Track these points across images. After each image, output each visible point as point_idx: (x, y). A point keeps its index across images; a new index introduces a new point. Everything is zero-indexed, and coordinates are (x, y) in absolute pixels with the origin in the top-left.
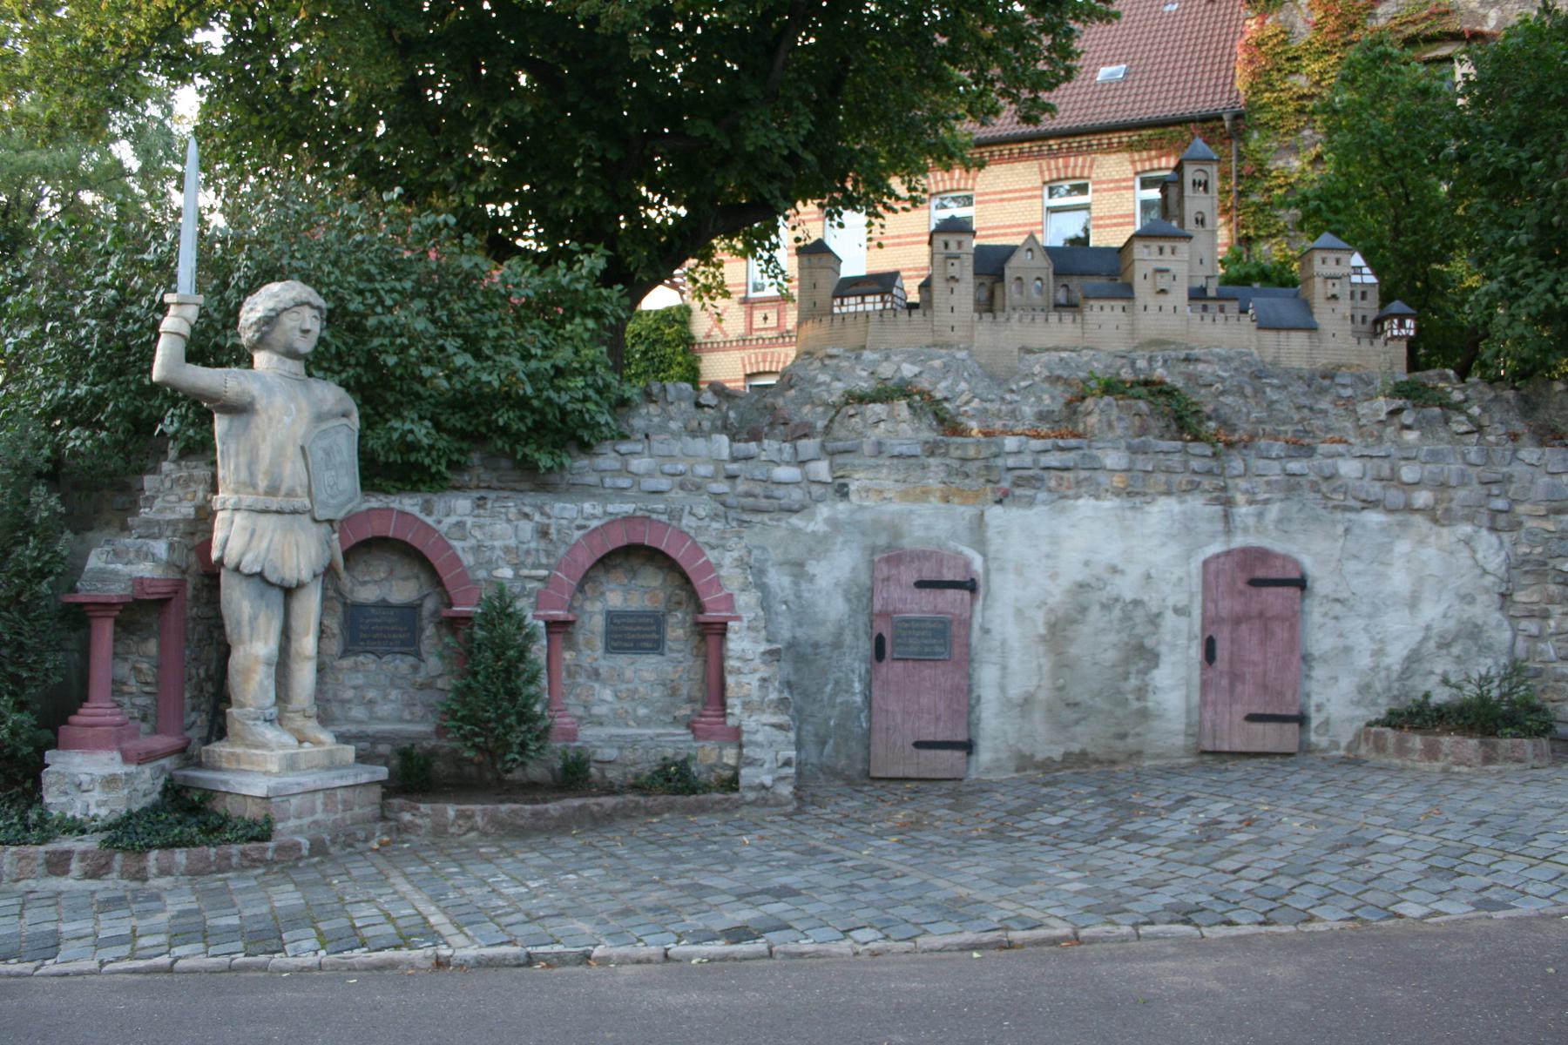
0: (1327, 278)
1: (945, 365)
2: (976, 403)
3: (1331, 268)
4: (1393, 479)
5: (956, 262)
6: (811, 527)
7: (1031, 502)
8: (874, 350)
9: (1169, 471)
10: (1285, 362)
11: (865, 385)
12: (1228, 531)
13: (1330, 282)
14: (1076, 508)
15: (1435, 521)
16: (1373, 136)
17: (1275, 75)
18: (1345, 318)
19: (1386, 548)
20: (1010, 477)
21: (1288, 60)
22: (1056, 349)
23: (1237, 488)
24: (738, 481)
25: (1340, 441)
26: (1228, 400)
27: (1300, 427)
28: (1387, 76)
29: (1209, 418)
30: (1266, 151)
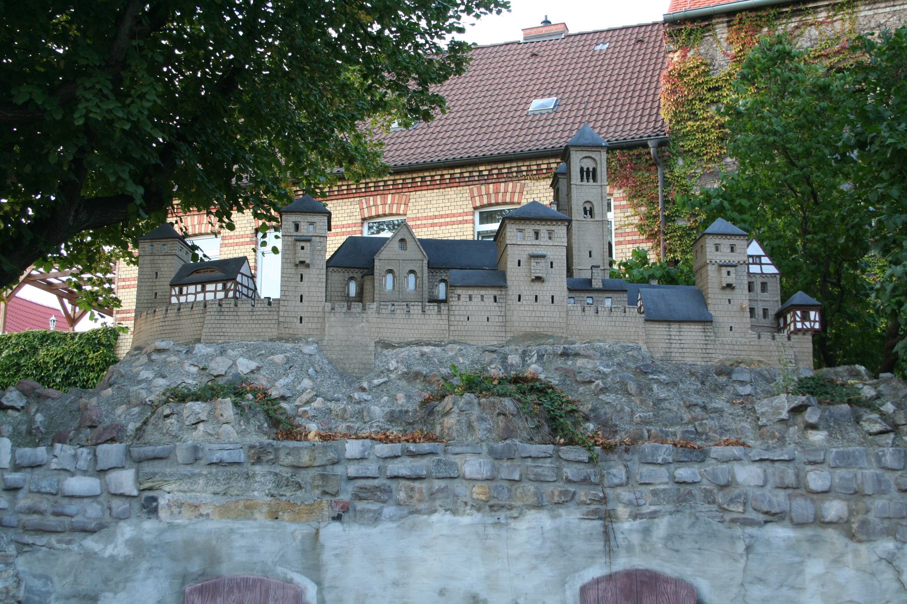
0: (721, 266)
1: (288, 360)
2: (318, 403)
3: (724, 255)
4: (798, 487)
5: (307, 245)
6: (109, 551)
7: (376, 518)
8: (209, 343)
9: (539, 480)
10: (676, 357)
11: (191, 380)
12: (609, 551)
13: (724, 270)
14: (430, 525)
15: (852, 536)
16: (775, 133)
17: (698, 105)
18: (742, 309)
19: (797, 569)
20: (350, 488)
21: (709, 90)
22: (418, 343)
23: (618, 499)
24: (21, 494)
25: (737, 443)
26: (610, 398)
27: (690, 428)
28: (787, 74)
29: (587, 419)
30: (691, 177)
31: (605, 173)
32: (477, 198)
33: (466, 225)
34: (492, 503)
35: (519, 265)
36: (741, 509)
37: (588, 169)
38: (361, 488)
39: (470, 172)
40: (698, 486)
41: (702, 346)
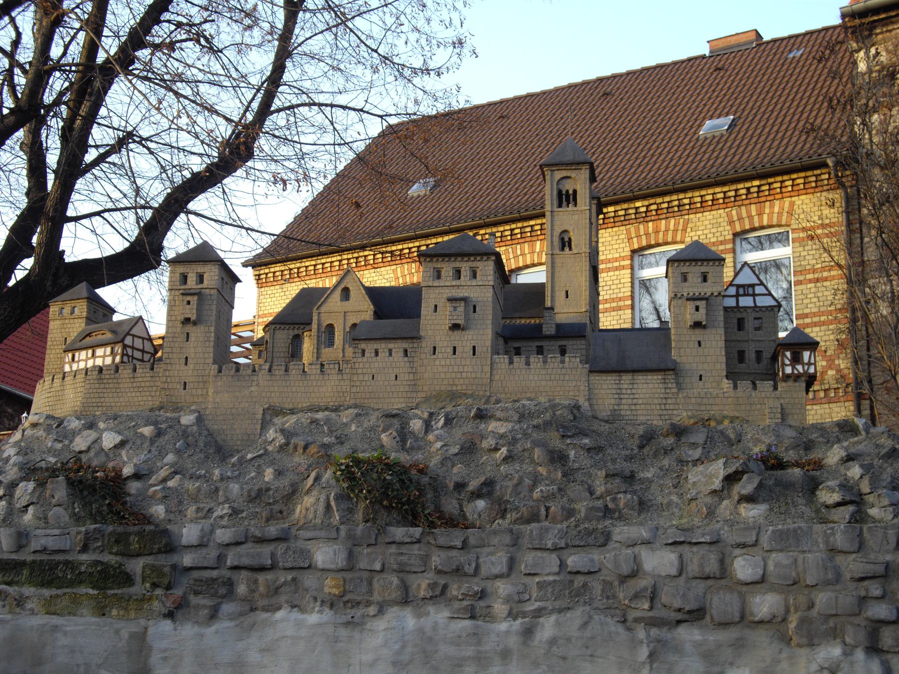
15: (786, 640)
22: (311, 409)
31: (548, 197)
32: (635, 240)
33: (623, 272)
34: (346, 598)
35: (436, 311)
36: (646, 606)
37: (567, 191)
38: (196, 580)
39: (625, 210)
40: (597, 576)
41: (660, 401)
